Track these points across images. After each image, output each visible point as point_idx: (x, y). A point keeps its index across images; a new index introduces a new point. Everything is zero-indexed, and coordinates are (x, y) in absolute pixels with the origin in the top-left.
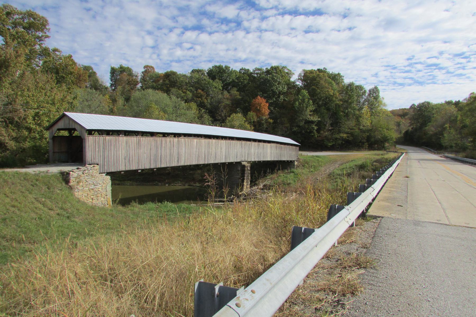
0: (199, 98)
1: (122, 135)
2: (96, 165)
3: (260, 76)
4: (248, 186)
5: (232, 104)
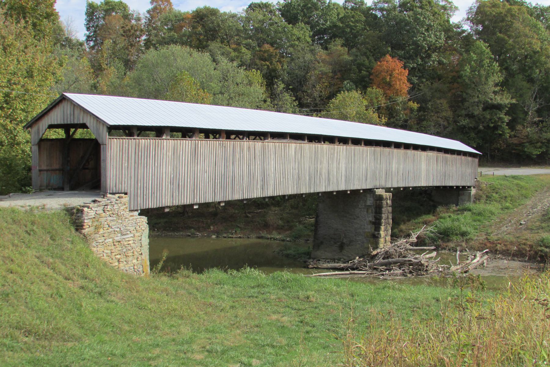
0: (265, 60)
1: (223, 138)
2: (123, 195)
3: (388, 15)
4: (388, 238)
5: (334, 72)
